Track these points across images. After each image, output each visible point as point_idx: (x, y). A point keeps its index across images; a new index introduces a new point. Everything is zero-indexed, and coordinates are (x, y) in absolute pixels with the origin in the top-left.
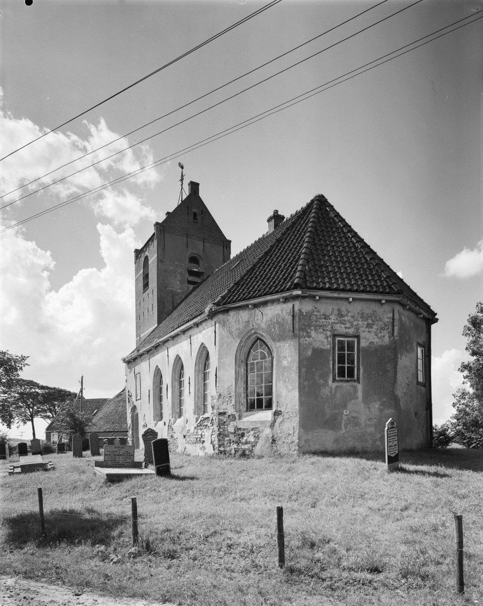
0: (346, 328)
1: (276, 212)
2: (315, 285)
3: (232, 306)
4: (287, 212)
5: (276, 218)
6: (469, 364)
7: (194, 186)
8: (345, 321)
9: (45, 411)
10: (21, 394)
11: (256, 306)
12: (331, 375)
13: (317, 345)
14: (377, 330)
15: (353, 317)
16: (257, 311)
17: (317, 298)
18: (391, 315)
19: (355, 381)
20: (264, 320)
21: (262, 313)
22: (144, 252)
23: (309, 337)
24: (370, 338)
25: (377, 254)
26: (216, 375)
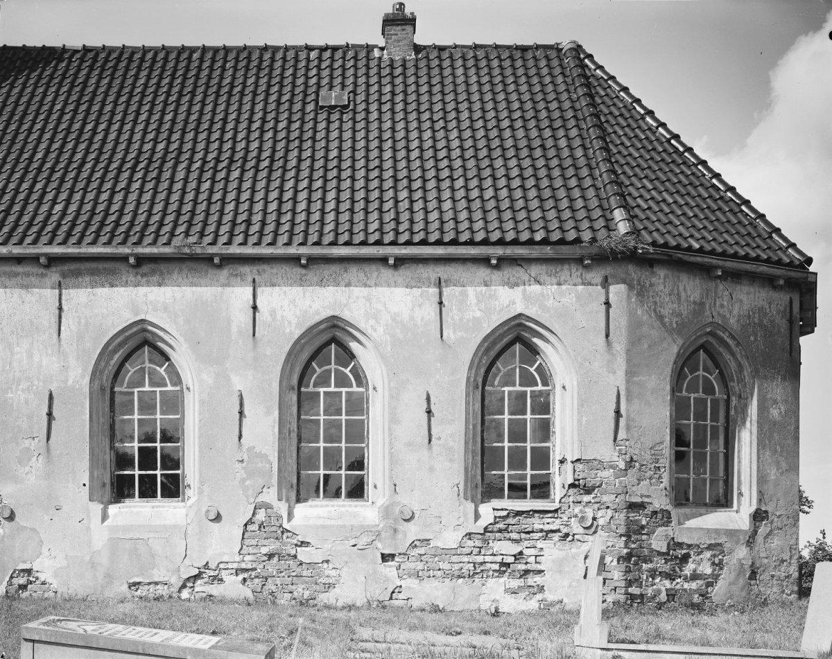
20: (735, 312)
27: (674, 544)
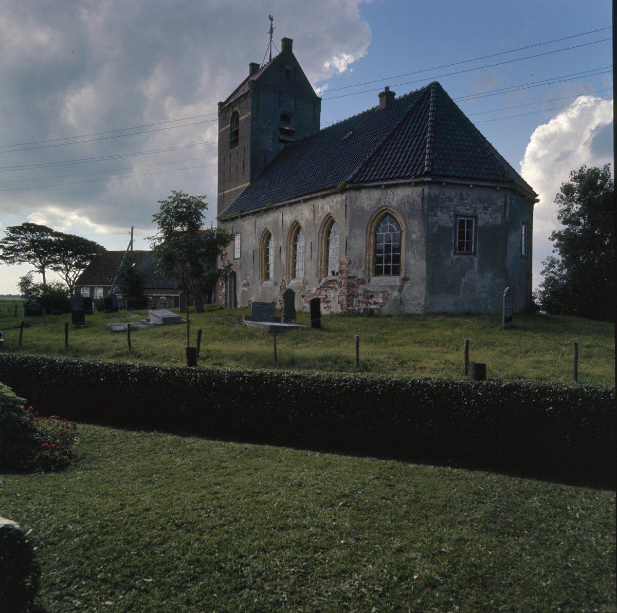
0: (466, 209)
1: (387, 88)
2: (442, 172)
3: (366, 185)
4: (400, 93)
5: (387, 95)
6: (560, 232)
7: (287, 44)
8: (465, 203)
9: (55, 262)
10: (32, 241)
11: (387, 187)
12: (453, 251)
13: (442, 223)
14: (492, 211)
15: (472, 200)
16: (389, 191)
17: (444, 184)
18: (503, 200)
19: (472, 254)
20: (395, 199)
21: (393, 193)
22: (233, 107)
23: (436, 216)
24: (486, 218)
25: (492, 145)
26: (346, 244)
27: (366, 291)
